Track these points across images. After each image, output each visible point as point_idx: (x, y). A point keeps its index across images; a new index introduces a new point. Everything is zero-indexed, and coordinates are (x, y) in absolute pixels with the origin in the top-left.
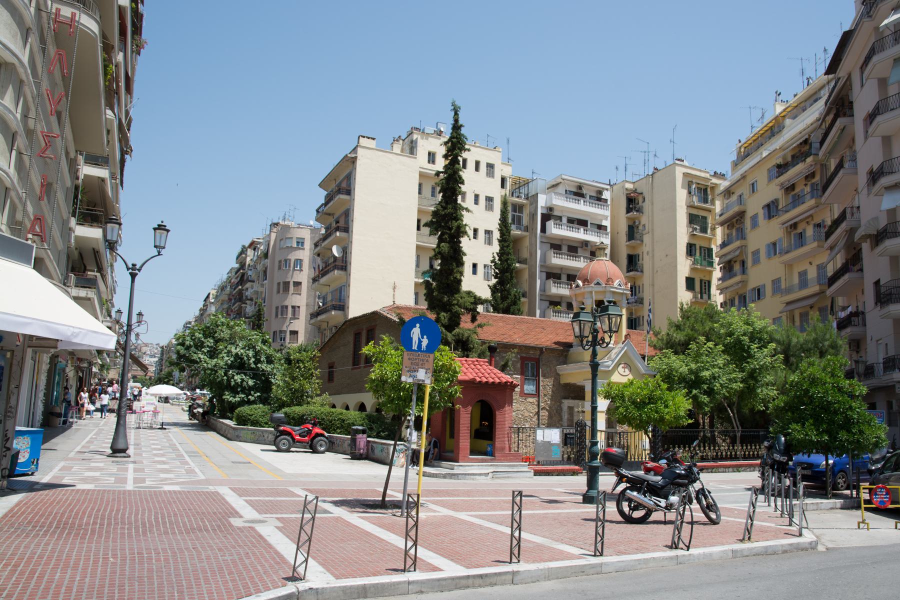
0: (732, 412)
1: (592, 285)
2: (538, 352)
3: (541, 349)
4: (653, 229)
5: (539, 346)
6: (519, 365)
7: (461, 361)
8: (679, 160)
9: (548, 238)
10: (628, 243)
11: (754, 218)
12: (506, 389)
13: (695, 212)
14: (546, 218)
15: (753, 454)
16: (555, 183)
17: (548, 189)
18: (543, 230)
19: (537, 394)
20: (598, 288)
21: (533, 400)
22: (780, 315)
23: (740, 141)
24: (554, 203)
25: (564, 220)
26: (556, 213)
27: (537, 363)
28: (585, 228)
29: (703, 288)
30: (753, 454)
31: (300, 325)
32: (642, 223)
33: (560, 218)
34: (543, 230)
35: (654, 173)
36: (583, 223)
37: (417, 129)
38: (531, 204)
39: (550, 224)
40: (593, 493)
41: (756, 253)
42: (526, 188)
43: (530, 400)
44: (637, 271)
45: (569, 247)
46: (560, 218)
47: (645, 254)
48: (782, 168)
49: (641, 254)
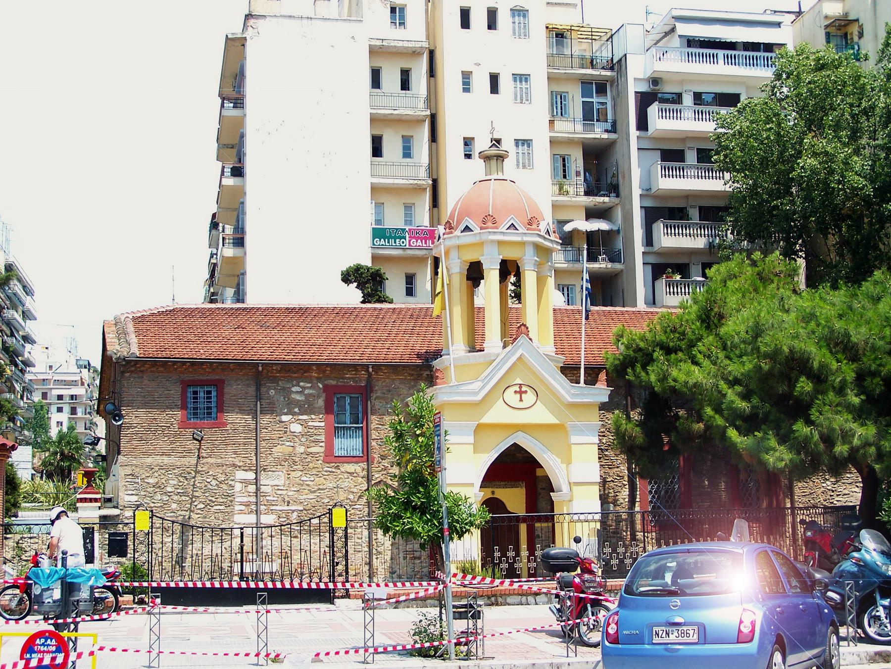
0: (347, 374)
1: (458, 233)
9: (653, 139)
12: (831, 573)
14: (645, 100)
18: (643, 124)
19: (366, 456)
20: (467, 238)
21: (358, 468)
26: (669, 88)
27: (366, 392)
33: (677, 99)
34: (643, 124)
39: (653, 110)
43: (350, 468)
45: (699, 151)
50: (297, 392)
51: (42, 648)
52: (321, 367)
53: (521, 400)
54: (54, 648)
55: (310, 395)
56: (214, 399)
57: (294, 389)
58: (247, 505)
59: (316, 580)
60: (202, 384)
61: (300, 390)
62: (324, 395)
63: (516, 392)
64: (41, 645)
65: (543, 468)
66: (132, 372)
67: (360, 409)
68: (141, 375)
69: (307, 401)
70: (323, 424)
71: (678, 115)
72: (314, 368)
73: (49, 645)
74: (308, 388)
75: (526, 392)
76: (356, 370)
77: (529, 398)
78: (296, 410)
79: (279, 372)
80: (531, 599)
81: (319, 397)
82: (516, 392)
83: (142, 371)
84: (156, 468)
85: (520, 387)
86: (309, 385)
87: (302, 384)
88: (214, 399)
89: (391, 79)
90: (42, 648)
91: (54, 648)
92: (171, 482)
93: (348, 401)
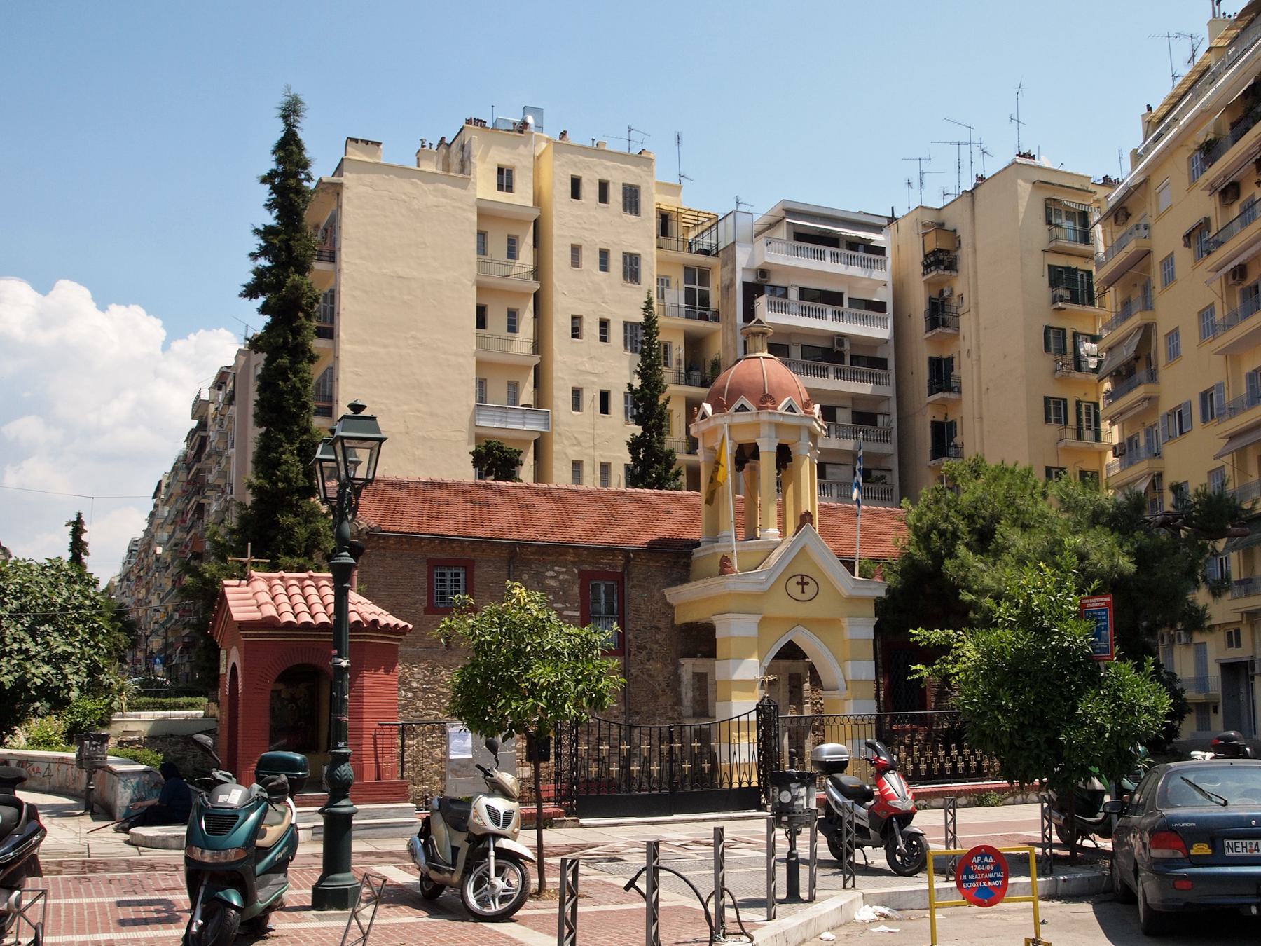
2: (620, 560)
3: (625, 552)
4: (977, 304)
5: (621, 546)
6: (576, 589)
7: (269, 580)
8: (1024, 156)
10: (929, 335)
11: (1169, 261)
13: (1061, 261)
14: (752, 291)
15: (967, 767)
16: (772, 220)
17: (756, 236)
18: (749, 314)
20: (741, 418)
22: (1218, 464)
23: (1149, 108)
24: (768, 260)
25: (793, 294)
26: (775, 281)
28: (837, 308)
29: (1084, 417)
30: (967, 767)
31: (919, 554)
32: (957, 292)
34: (749, 314)
35: (976, 187)
36: (833, 298)
37: (479, 122)
38: (724, 265)
39: (762, 303)
40: (343, 880)
41: (1173, 335)
42: (714, 233)
44: (950, 390)
46: (785, 292)
47: (964, 355)
48: (1210, 150)
49: (956, 355)
50: (552, 577)
51: (979, 868)
52: (577, 549)
53: (803, 592)
54: (992, 867)
55: (566, 580)
56: (462, 583)
57: (549, 574)
60: (449, 563)
62: (579, 581)
63: (798, 583)
64: (977, 864)
66: (372, 548)
68: (382, 551)
69: (562, 587)
70: (578, 614)
71: (784, 309)
72: (571, 551)
73: (987, 863)
74: (562, 573)
75: (807, 583)
76: (614, 555)
77: (810, 590)
79: (533, 554)
81: (574, 583)
82: (798, 583)
83: (383, 548)
85: (802, 578)
86: (564, 570)
87: (556, 568)
88: (462, 583)
89: (498, 248)
90: (979, 868)
91: (992, 867)
92: (416, 676)
93: (603, 588)
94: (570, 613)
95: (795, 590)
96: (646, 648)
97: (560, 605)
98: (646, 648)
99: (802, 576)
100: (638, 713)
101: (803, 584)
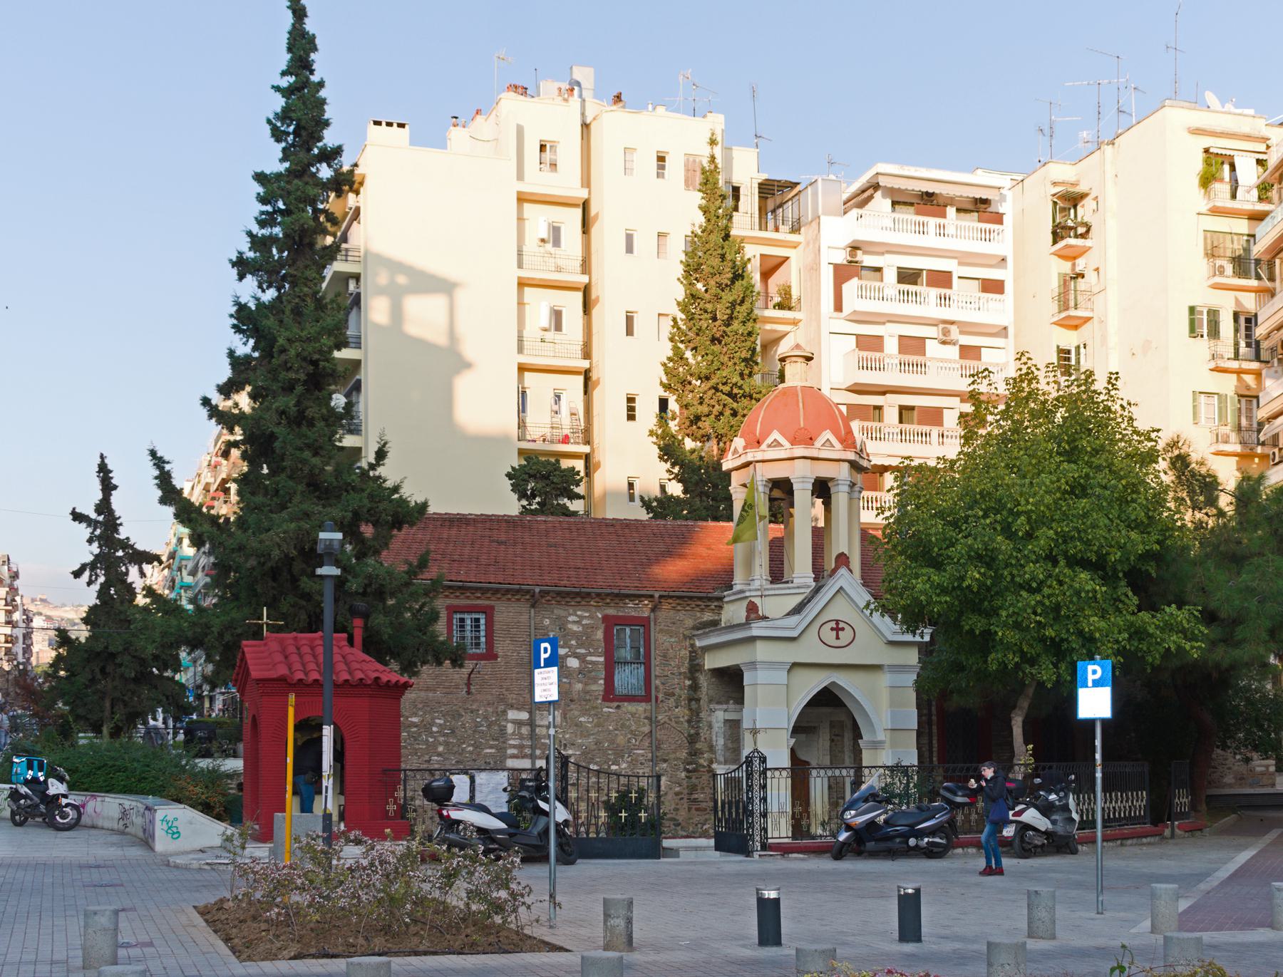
6: (600, 634)
53: (838, 638)
56: (483, 627)
57: (571, 618)
58: (521, 747)
59: (593, 829)
60: (470, 610)
61: (575, 619)
63: (832, 629)
65: (845, 706)
67: (642, 642)
70: (602, 659)
75: (843, 629)
77: (846, 636)
78: (573, 642)
80: (101, 863)
82: (832, 629)
84: (420, 706)
86: (587, 614)
87: (579, 613)
88: (483, 627)
92: (438, 721)
93: (628, 630)
94: (594, 659)
95: (829, 636)
96: (674, 695)
97: (583, 651)
98: (674, 695)
99: (837, 622)
100: (665, 761)
101: (837, 629)
